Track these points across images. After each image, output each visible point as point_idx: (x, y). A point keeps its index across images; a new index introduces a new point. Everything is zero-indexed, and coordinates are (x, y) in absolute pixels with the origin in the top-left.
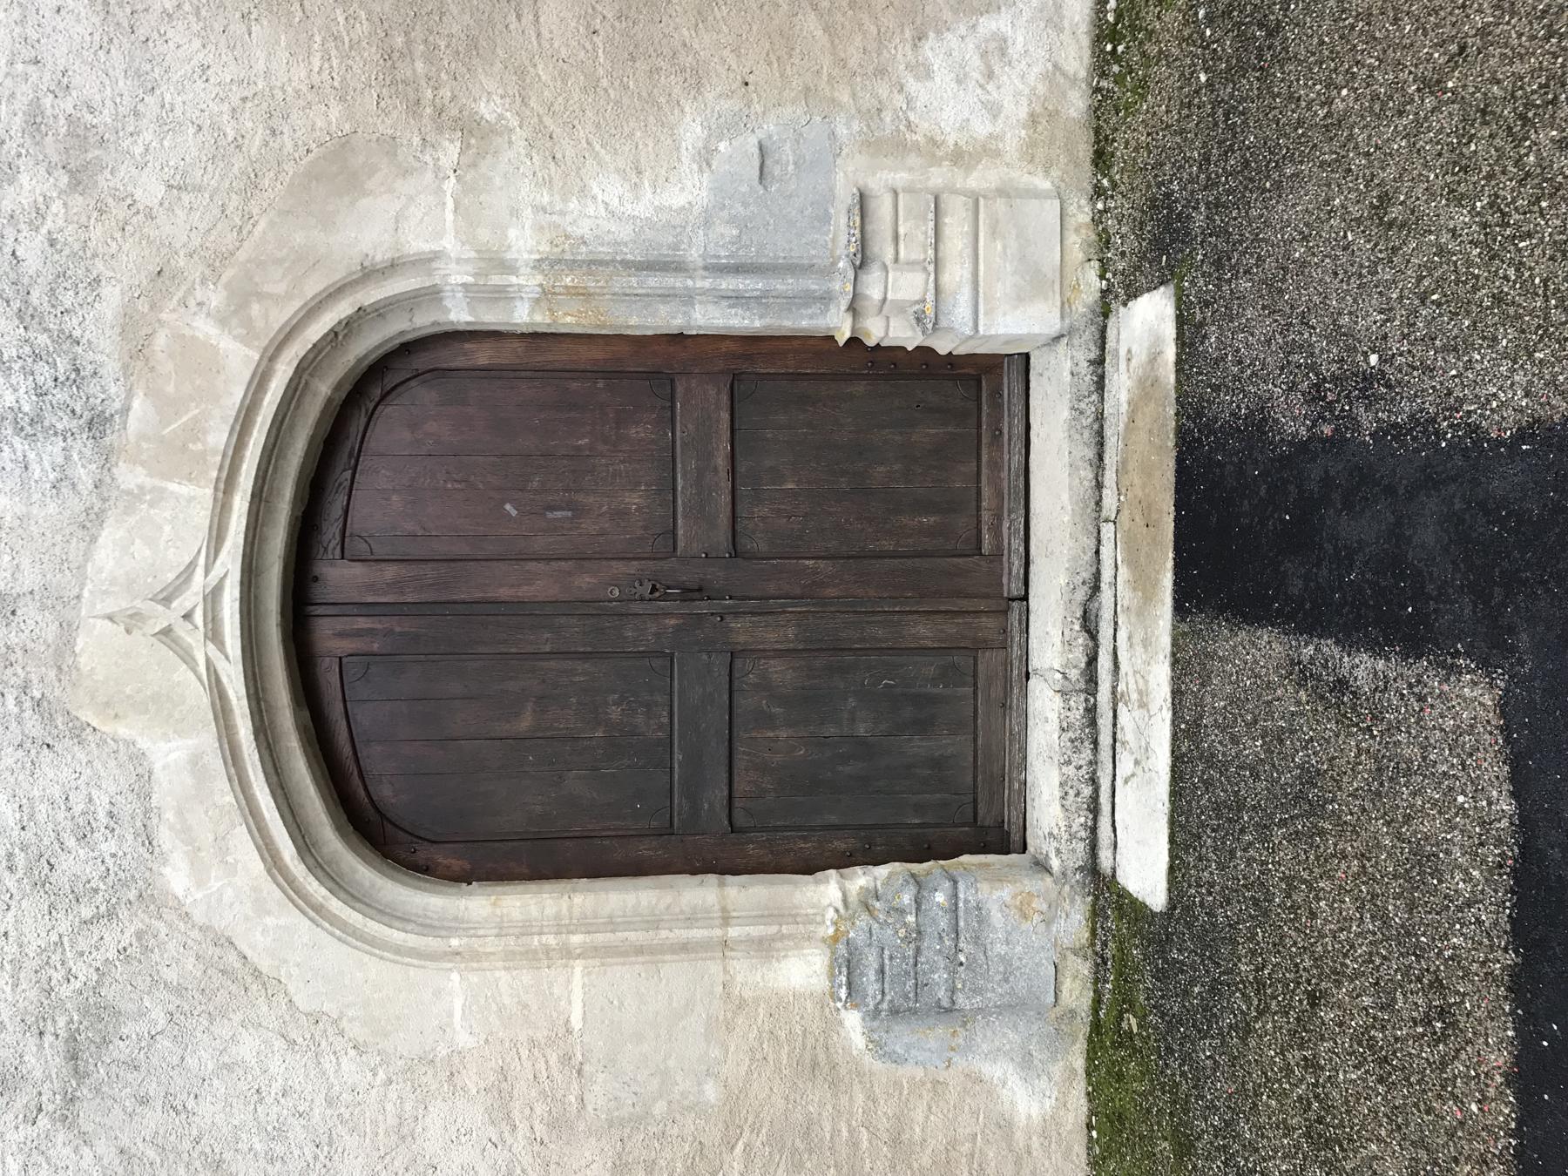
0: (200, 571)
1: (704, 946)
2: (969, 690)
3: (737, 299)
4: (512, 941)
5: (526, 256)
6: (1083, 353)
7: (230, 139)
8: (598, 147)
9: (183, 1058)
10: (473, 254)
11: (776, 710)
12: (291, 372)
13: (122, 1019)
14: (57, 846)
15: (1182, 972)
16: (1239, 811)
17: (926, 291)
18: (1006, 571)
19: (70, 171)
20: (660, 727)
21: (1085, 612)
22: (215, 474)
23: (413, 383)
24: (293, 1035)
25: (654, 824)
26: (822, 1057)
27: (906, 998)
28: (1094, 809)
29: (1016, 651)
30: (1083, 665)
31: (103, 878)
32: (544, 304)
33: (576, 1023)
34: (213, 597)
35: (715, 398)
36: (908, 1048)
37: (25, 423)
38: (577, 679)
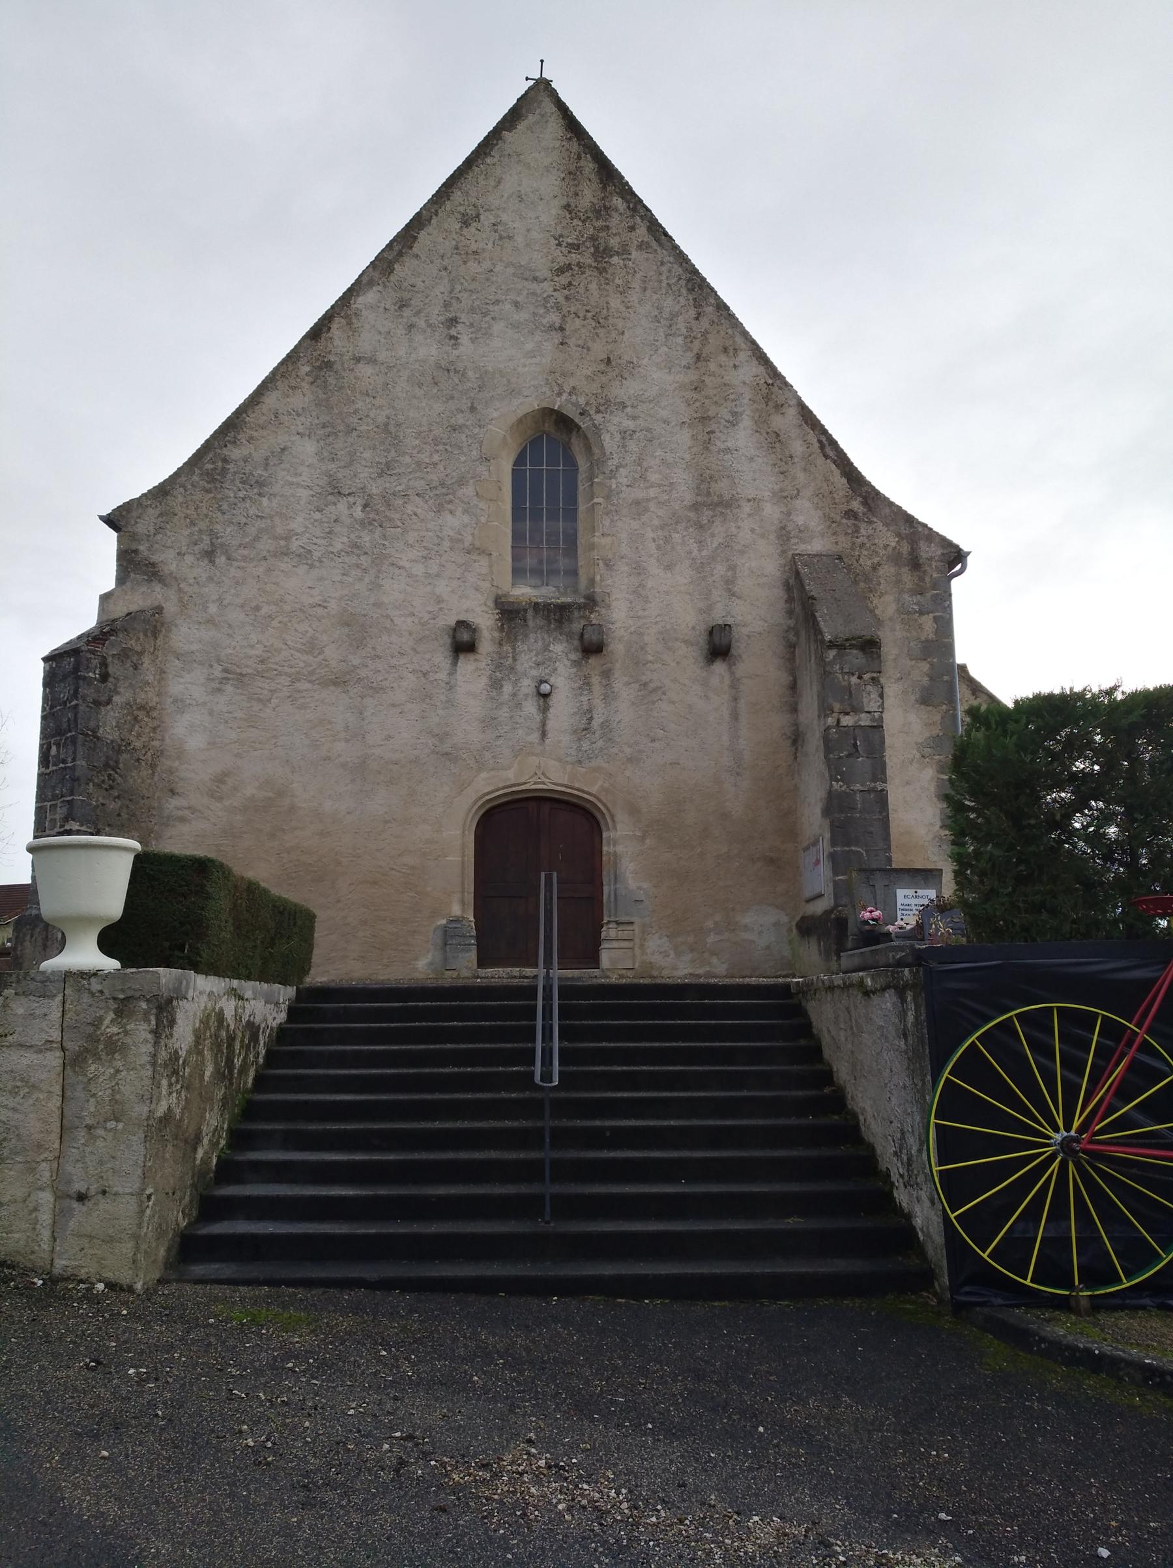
1: (463, 888)
34: (544, 783)
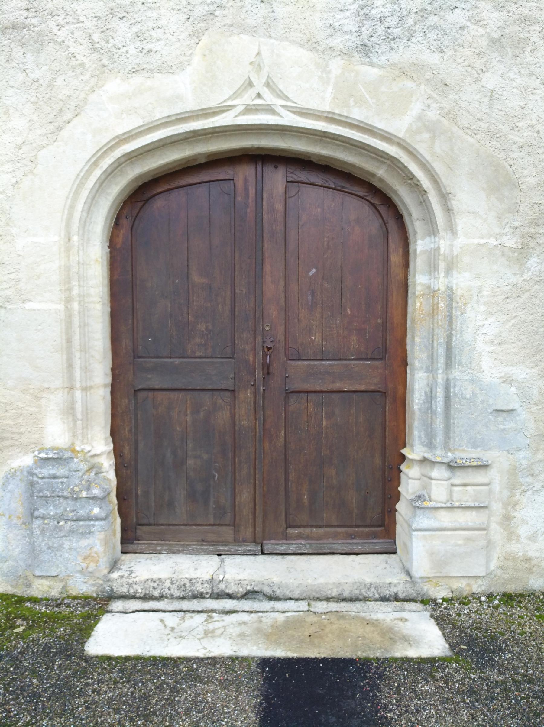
0: (284, 103)
2: (212, 521)
3: (430, 397)
4: (75, 270)
5: (455, 282)
6: (401, 590)
7: (518, 124)
8: (513, 321)
9: (12, 87)
10: (455, 253)
11: (202, 415)
12: (392, 154)
13: (35, 54)
14: (133, 21)
15: (47, 669)
16: (144, 716)
17: (436, 502)
18: (277, 542)
19: (500, 39)
20: (194, 352)
21: (257, 592)
22: (337, 111)
23: (381, 221)
24: (24, 148)
25: (140, 348)
26: (7, 443)
27: (40, 491)
28: (146, 598)
29: (233, 548)
30: (227, 591)
31: (114, 46)
32: (427, 291)
33: (28, 305)
34: (269, 110)
35: (372, 382)
36: (11, 492)
37: (365, 10)
38: (220, 306)
